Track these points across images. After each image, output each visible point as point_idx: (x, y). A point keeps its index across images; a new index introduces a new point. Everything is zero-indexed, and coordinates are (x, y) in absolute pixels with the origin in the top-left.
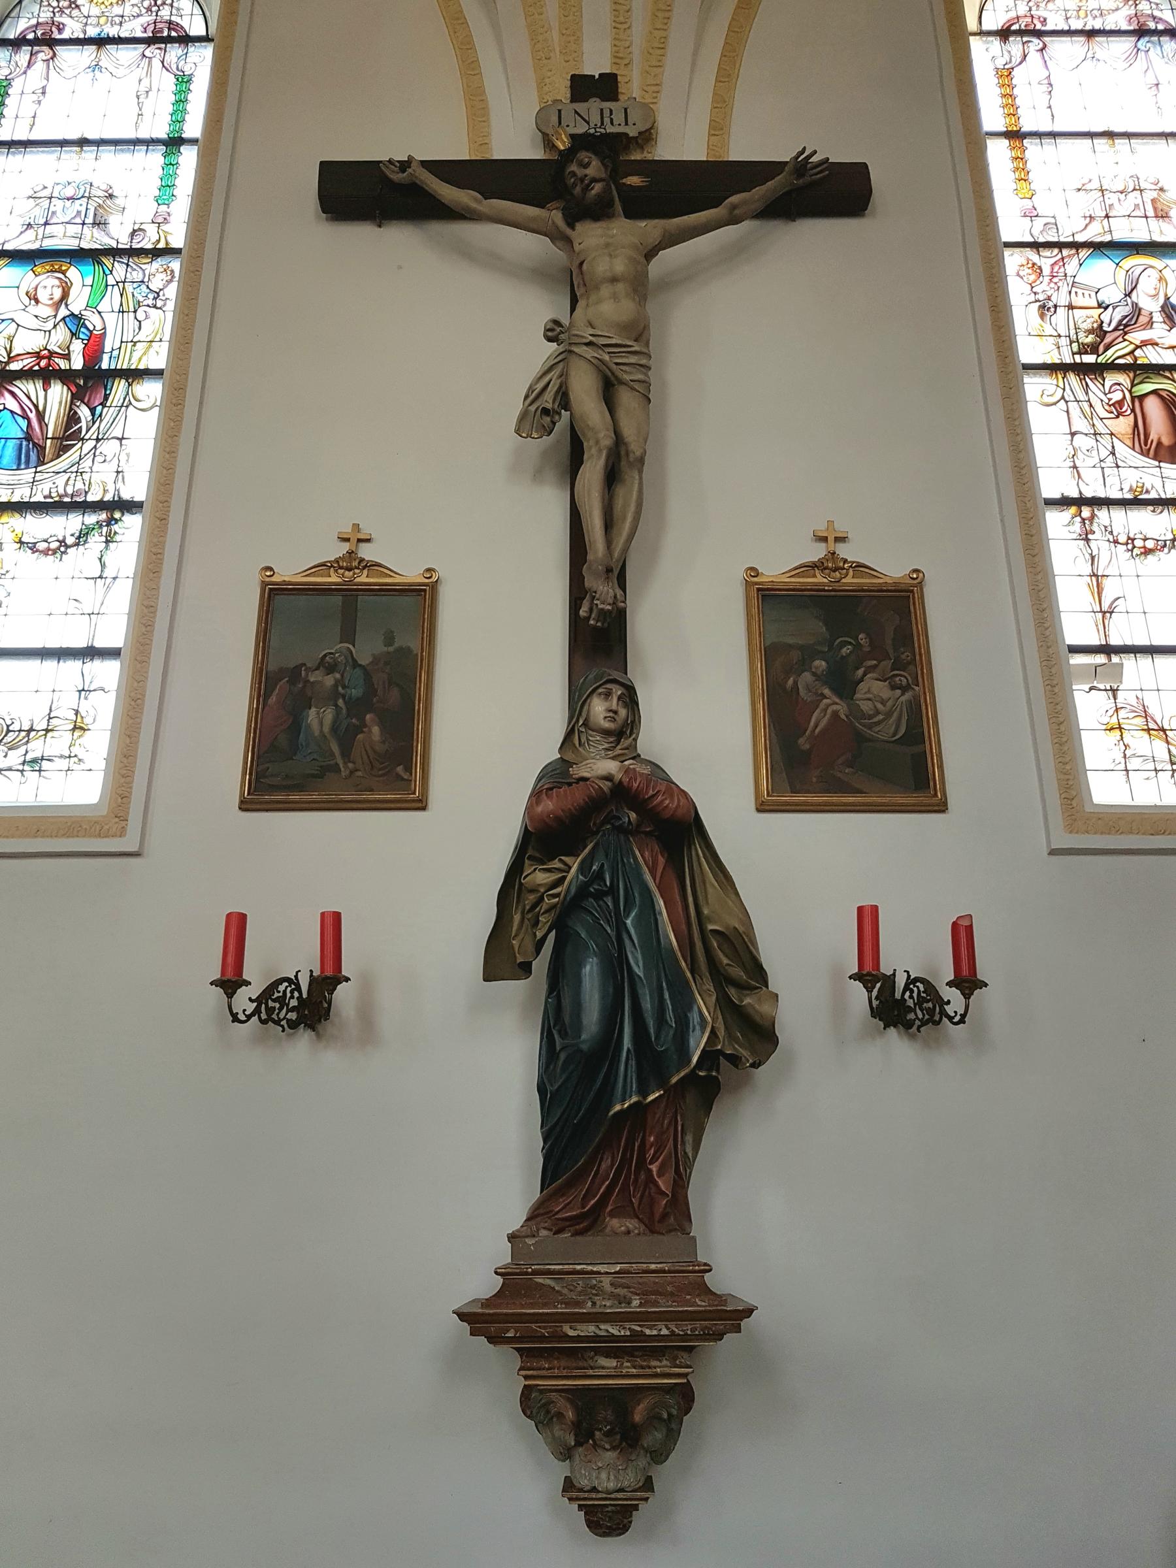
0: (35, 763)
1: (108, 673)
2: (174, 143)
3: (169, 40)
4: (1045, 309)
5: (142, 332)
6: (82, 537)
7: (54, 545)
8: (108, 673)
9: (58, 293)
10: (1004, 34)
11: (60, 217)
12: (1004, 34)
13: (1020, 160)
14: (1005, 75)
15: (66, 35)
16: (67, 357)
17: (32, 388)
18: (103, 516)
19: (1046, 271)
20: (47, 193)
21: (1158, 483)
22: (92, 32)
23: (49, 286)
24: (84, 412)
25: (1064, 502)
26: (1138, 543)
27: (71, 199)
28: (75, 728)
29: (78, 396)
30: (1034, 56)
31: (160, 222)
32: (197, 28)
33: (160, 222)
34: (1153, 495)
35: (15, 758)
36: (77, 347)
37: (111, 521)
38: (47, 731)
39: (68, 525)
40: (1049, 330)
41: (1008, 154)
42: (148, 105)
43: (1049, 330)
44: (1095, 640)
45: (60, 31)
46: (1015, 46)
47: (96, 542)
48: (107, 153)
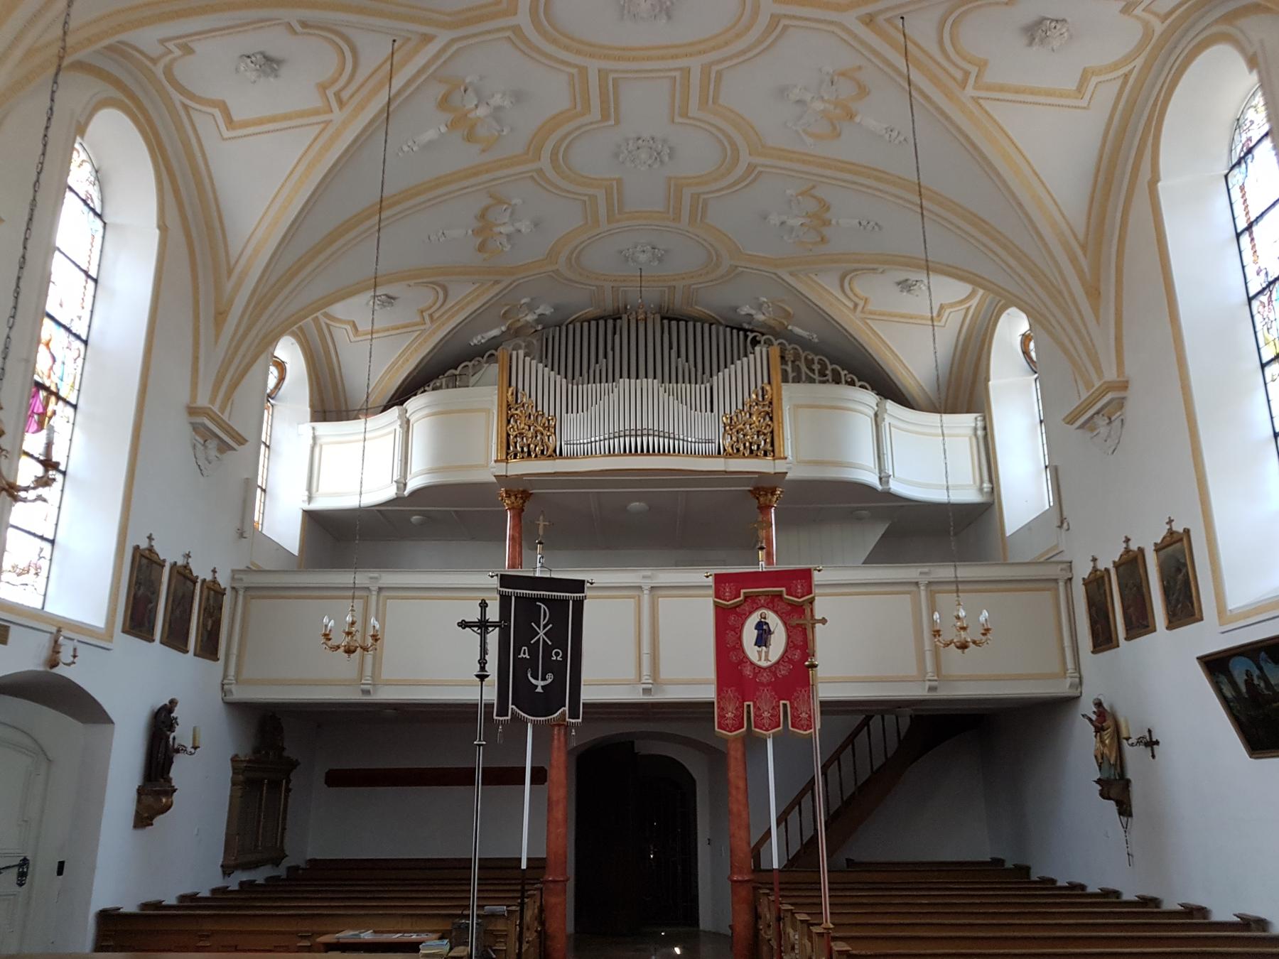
2: (1249, 228)
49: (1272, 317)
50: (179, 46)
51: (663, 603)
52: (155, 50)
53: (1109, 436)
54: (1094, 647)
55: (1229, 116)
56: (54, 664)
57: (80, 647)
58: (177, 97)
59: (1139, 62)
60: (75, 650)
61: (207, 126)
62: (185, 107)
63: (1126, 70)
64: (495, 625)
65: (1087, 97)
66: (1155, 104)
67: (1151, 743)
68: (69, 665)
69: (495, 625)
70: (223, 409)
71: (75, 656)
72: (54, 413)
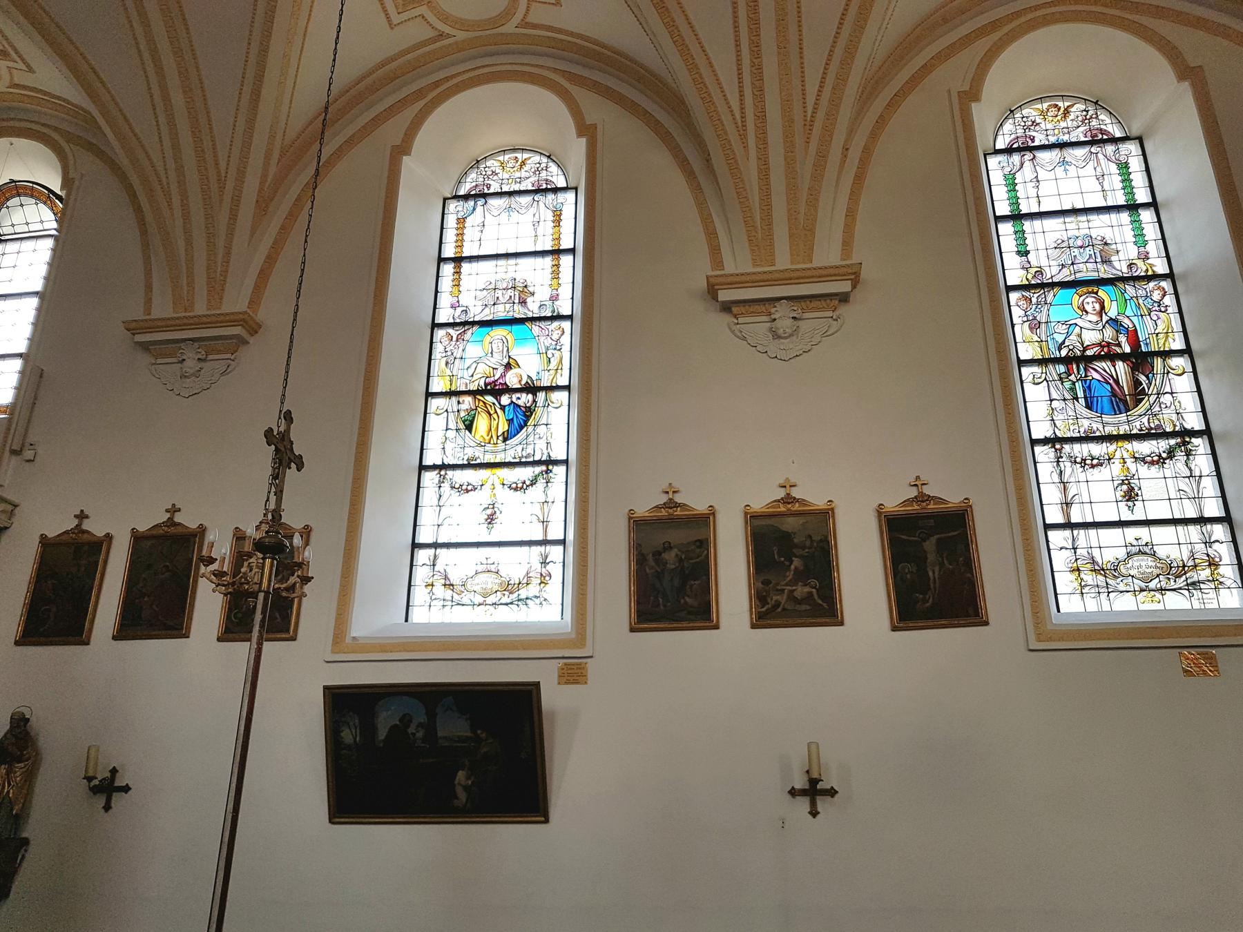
0: (1195, 585)
2: (458, 260)
3: (546, 190)
4: (1035, 326)
5: (1162, 330)
6: (1171, 454)
9: (1097, 306)
10: (1009, 151)
11: (1080, 259)
12: (1009, 151)
13: (1020, 235)
15: (492, 191)
16: (1119, 345)
17: (1105, 365)
18: (544, 468)
19: (1034, 300)
20: (492, 286)
22: (1052, 140)
23: (1091, 304)
24: (1142, 378)
25: (1045, 441)
26: (1088, 462)
28: (1210, 565)
29: (1135, 369)
31: (554, 298)
32: (561, 183)
33: (554, 298)
34: (1098, 434)
35: (1181, 582)
36: (1123, 339)
37: (1185, 443)
39: (526, 473)
40: (1036, 338)
42: (540, 231)
43: (1036, 338)
44: (540, 537)
45: (1033, 141)
46: (1016, 158)
47: (541, 484)
48: (523, 261)
49: (458, 354)
51: (1050, 533)
53: (197, 374)
54: (760, 616)
55: (476, 151)
59: (461, 36)
63: (447, 29)
64: (1145, 206)
65: (405, 16)
66: (437, 84)
67: (107, 788)
69: (1145, 206)
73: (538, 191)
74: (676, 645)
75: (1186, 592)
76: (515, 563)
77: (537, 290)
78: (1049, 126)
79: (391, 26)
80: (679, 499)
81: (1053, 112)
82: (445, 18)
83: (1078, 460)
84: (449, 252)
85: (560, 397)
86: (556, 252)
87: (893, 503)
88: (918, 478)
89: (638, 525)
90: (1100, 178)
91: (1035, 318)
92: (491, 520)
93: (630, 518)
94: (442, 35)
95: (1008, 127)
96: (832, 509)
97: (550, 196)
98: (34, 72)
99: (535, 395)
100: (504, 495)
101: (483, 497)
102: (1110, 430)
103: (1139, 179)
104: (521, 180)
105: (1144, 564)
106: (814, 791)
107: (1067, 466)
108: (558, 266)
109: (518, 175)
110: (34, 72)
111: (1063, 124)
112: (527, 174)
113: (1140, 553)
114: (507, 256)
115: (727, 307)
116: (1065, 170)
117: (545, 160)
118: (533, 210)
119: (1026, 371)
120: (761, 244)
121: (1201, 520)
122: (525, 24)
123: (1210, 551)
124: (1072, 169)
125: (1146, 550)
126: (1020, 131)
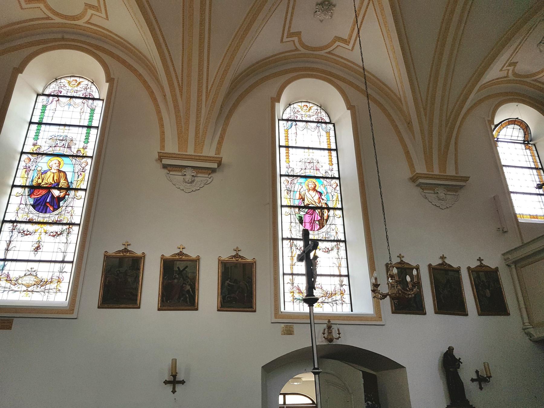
1: (68, 267)
3: (89, 99)
4: (289, 191)
7: (55, 234)
8: (68, 267)
12: (287, 120)
14: (287, 131)
15: (62, 94)
19: (32, 160)
20: (55, 138)
21: (36, 218)
26: (25, 233)
27: (62, 140)
30: (294, 127)
32: (97, 96)
33: (85, 148)
35: (330, 300)
38: (51, 282)
39: (57, 228)
41: (285, 152)
44: (338, 274)
45: (61, 93)
50: (510, 65)
52: (504, 74)
54: (222, 306)
56: (331, 340)
57: (341, 327)
58: (322, 53)
59: (303, 51)
60: (338, 330)
61: (344, 51)
62: (329, 53)
63: (51, 15)
68: (338, 339)
70: (443, 164)
71: (339, 334)
72: (328, 216)
73: (85, 98)
74: (179, 317)
75: (331, 304)
76: (45, 271)
77: (77, 143)
78: (303, 113)
79: (282, 41)
80: (129, 248)
81: (74, 83)
82: (50, 9)
83: (22, 231)
84: (36, 119)
85: (82, 194)
86: (89, 127)
87: (225, 257)
88: (237, 248)
89: (107, 258)
90: (82, 112)
91: (29, 167)
92: (37, 249)
93: (219, 260)
94: (48, 18)
95: (53, 85)
96: (255, 262)
97: (90, 101)
98: (108, 20)
99: (314, 210)
100: (46, 238)
101: (35, 238)
102: (41, 220)
103: (333, 139)
104: (77, 91)
105: (30, 280)
106: (174, 382)
107: (294, 248)
108: (39, 130)
109: (76, 89)
110: (108, 20)
111: (308, 113)
112: (313, 114)
113: (30, 274)
114: (65, 125)
115: (165, 166)
116: (69, 108)
117: (90, 83)
118: (317, 130)
119: (284, 209)
120: (182, 140)
121: (340, 276)
122: (88, 22)
123: (342, 288)
124: (71, 107)
125: (31, 273)
126: (57, 88)
